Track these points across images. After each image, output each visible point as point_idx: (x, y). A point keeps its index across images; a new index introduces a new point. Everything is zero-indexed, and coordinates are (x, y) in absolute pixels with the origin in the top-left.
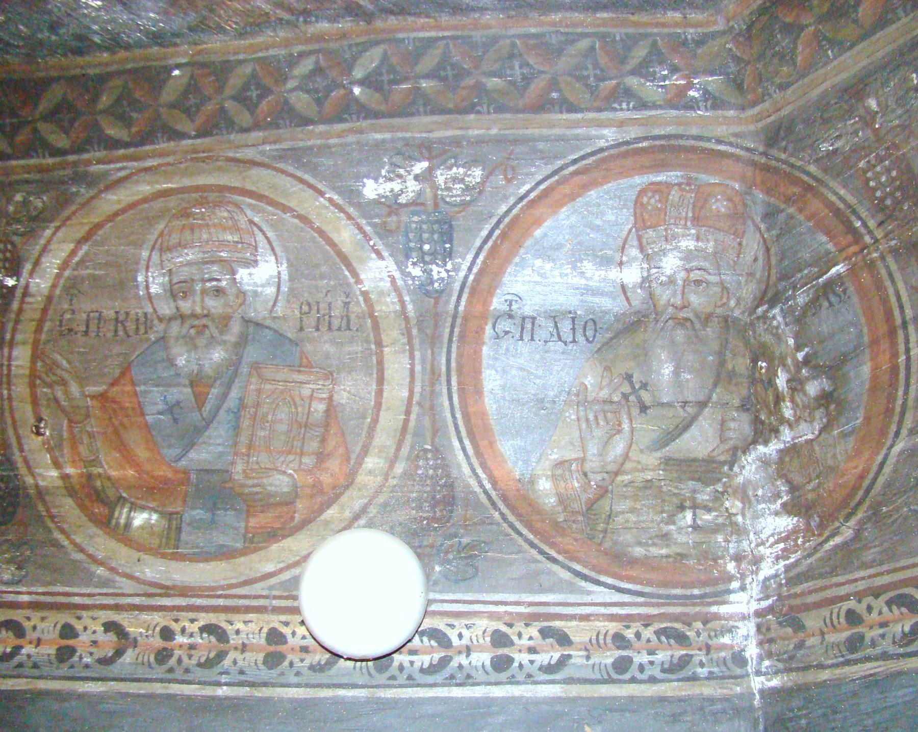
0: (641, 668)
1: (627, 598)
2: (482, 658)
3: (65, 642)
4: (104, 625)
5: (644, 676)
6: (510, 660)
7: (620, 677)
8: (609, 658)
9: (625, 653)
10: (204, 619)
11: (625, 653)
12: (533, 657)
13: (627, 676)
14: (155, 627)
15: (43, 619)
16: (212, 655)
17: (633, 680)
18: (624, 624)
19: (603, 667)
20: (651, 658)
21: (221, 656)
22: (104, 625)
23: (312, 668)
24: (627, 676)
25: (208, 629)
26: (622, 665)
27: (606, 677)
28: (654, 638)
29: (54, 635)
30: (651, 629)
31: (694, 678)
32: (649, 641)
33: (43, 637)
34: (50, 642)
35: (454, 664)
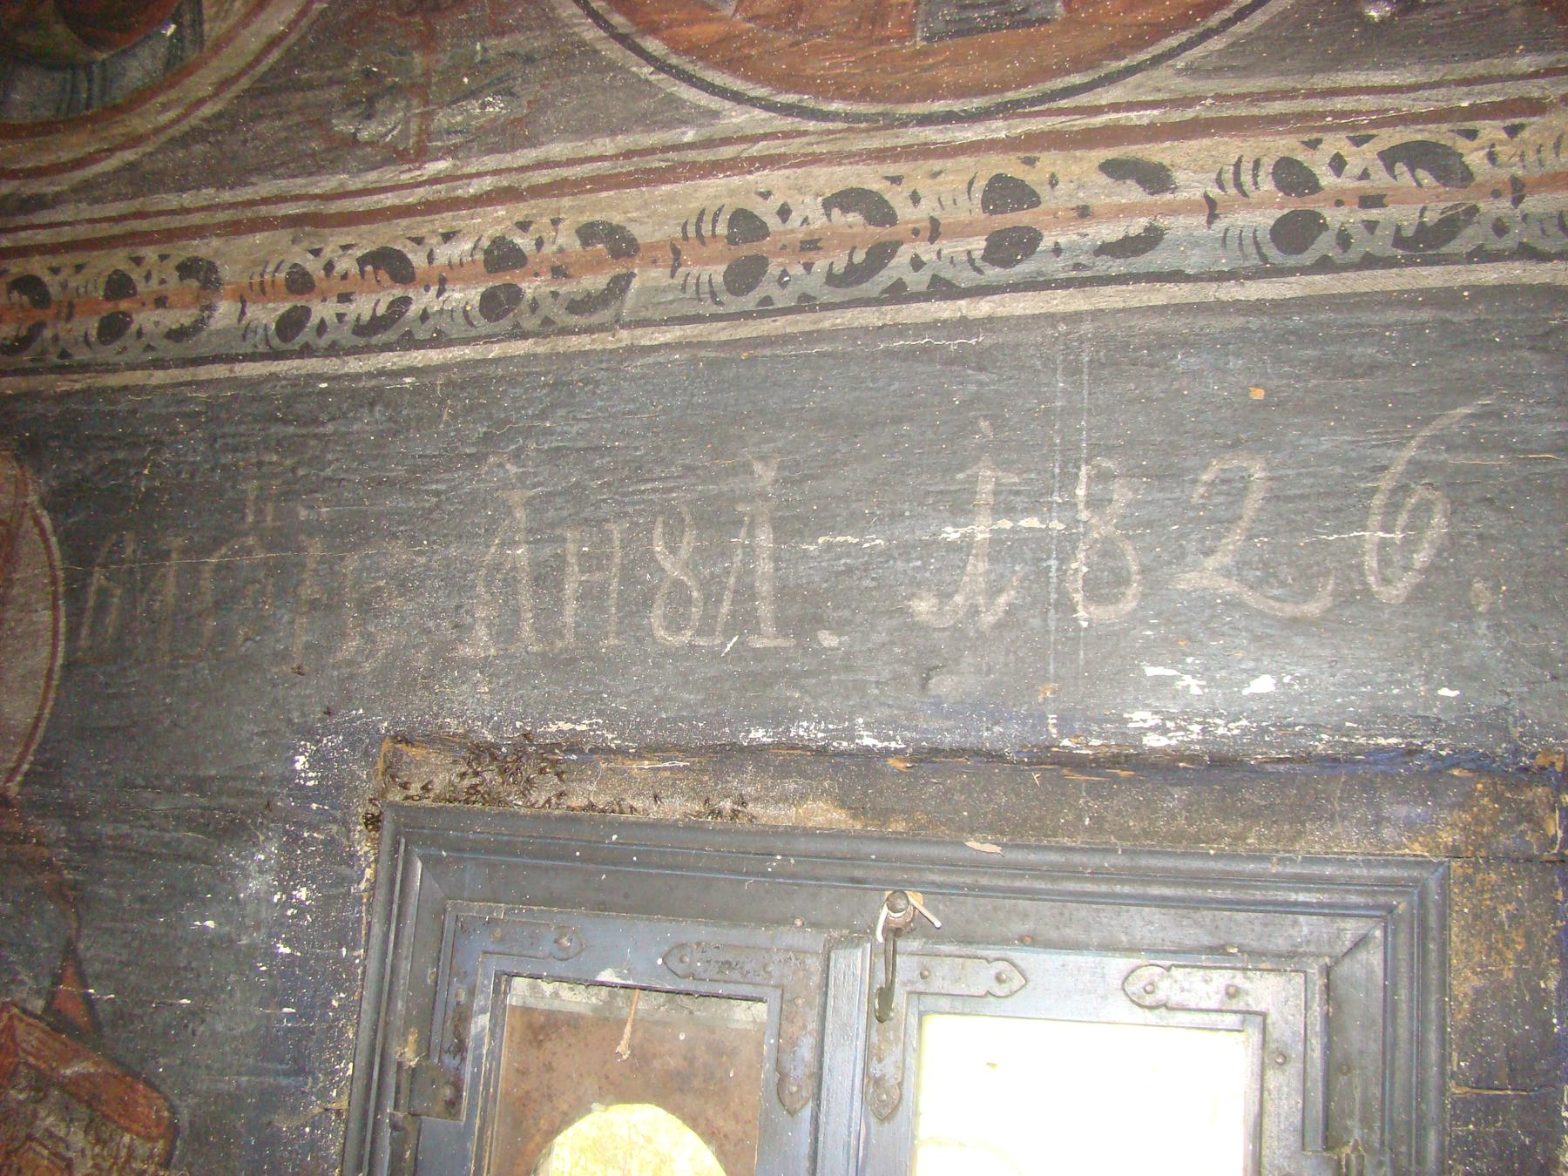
0: (1500, 229)
1: (787, 123)
2: (466, 296)
3: (745, 250)
4: (180, 268)
6: (515, 294)
7: (1292, 261)
8: (266, 314)
9: (300, 302)
10: (368, 239)
11: (300, 302)
12: (1374, 214)
13: (1308, 258)
14: (1237, 174)
15: (79, 268)
16: (859, 257)
17: (1324, 265)
18: (1508, 122)
19: (1248, 241)
20: (341, 308)
21: (881, 254)
22: (180, 268)
23: (832, 279)
24: (1308, 258)
25: (846, 200)
26: (291, 324)
27: (1255, 261)
28: (354, 269)
29: (969, 209)
30: (1370, 150)
31: (897, 293)
32: (345, 277)
33: (945, 218)
34: (964, 231)
35: (414, 310)
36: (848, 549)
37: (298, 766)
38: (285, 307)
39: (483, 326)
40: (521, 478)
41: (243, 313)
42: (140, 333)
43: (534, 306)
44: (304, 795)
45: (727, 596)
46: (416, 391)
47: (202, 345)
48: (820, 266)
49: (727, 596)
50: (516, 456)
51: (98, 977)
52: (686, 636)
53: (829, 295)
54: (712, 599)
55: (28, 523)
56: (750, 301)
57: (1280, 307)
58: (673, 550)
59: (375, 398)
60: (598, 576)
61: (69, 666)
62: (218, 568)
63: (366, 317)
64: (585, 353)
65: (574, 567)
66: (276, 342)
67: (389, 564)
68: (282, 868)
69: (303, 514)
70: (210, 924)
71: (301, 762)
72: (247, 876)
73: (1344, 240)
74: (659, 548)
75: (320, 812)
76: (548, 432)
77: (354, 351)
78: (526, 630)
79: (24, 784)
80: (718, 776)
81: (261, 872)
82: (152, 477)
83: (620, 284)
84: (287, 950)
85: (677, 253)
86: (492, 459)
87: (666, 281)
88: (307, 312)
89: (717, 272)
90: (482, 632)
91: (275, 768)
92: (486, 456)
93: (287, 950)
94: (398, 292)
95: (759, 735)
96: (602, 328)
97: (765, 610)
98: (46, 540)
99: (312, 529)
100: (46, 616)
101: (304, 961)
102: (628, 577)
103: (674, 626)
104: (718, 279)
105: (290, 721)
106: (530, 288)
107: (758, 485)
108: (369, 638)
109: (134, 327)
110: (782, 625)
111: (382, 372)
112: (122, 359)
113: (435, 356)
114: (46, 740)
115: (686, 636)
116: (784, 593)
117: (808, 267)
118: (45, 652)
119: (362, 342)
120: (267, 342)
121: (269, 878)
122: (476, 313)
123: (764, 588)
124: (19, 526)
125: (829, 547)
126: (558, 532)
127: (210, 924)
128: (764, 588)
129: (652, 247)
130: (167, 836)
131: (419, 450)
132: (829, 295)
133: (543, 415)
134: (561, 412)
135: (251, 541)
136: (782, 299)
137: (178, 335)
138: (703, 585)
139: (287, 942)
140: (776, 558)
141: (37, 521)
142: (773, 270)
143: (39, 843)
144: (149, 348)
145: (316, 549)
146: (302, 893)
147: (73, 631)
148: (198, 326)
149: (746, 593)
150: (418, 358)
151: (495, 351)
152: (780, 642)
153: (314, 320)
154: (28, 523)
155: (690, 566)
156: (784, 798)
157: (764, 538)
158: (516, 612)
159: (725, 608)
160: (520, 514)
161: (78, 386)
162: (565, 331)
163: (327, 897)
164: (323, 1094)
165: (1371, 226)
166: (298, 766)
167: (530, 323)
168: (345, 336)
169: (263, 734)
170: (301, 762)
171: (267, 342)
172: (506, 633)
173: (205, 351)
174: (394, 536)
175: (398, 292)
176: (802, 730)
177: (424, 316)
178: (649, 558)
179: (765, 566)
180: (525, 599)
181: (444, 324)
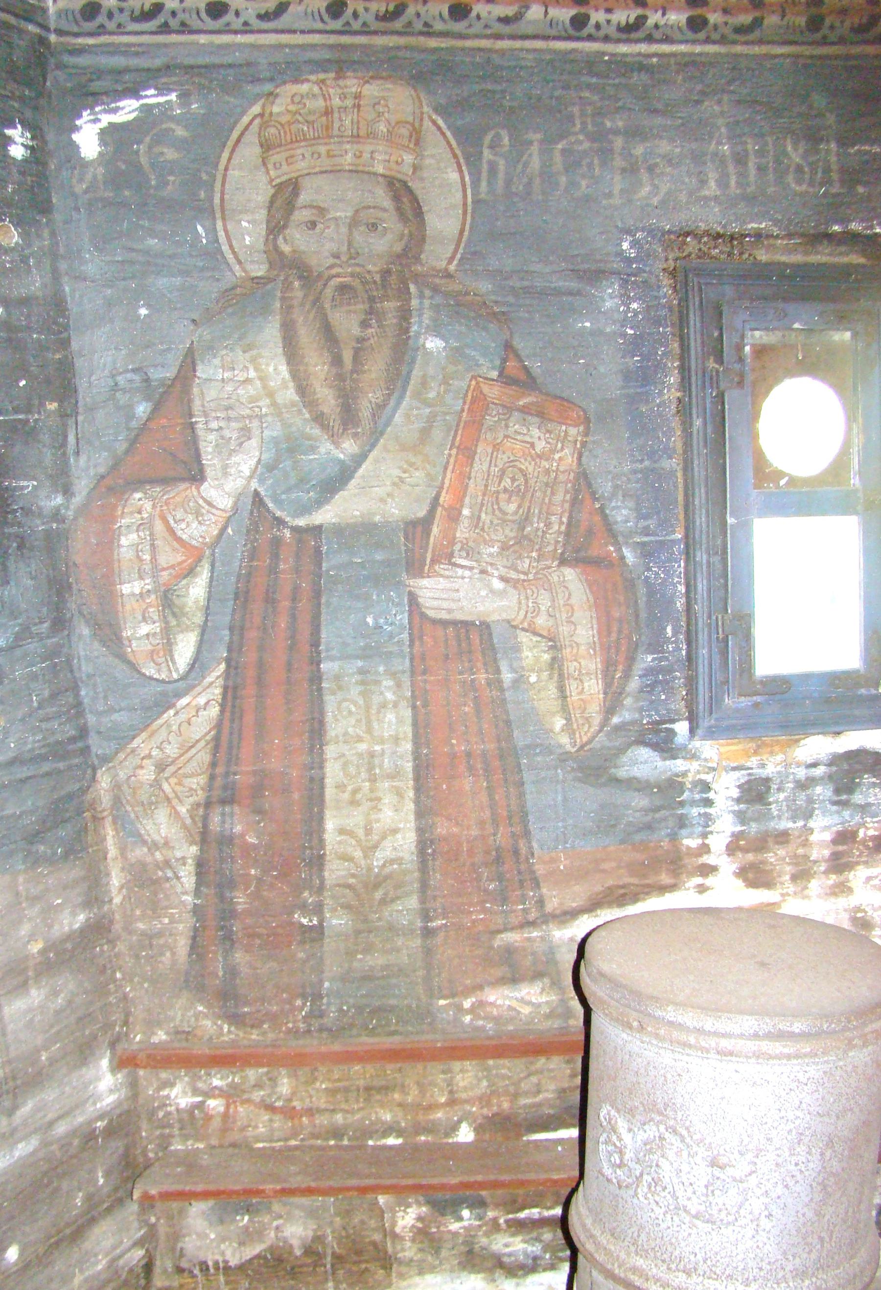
5: (602, 33)
6: (705, 22)
9: (583, 10)
11: (583, 10)
26: (579, 22)
35: (650, 22)
36: (866, 153)
37: (624, 248)
38: (573, 12)
39: (690, 35)
40: (722, 113)
41: (546, 12)
42: (478, 17)
43: (716, 27)
44: (629, 261)
45: (820, 170)
46: (660, 66)
47: (522, 27)
48: (848, 24)
49: (820, 170)
50: (719, 102)
51: (528, 357)
52: (804, 187)
53: (256, 24)
54: (813, 171)
55: (427, 123)
56: (818, 36)
57: (828, 57)
58: (796, 150)
59: (642, 68)
60: (764, 160)
61: (477, 202)
62: (563, 151)
63: (623, 23)
64: (747, 55)
65: (752, 157)
66: (571, 32)
67: (661, 151)
68: (622, 295)
69: (609, 124)
70: (588, 324)
71: (625, 246)
72: (604, 301)
73: (598, 26)
74: (789, 148)
75: (638, 268)
76: (733, 92)
77: (618, 41)
78: (733, 183)
79: (458, 265)
80: (813, 246)
81: (611, 298)
82: (511, 100)
83: (757, 23)
84: (632, 332)
85: (784, 11)
86: (706, 103)
87: (779, 22)
88: (587, 17)
89: (801, 21)
90: (712, 184)
91: (611, 249)
92: (703, 101)
93: (632, 332)
94: (639, 11)
95: (836, 228)
96: (752, 43)
97: (835, 176)
98: (443, 134)
99: (616, 132)
100: (454, 176)
101: (641, 337)
102: (778, 162)
103: (799, 182)
104: (803, 24)
105: (617, 227)
106: (714, 18)
107: (828, 123)
108: (656, 187)
109: (474, 14)
110: (842, 181)
111: (639, 54)
112: (471, 31)
113: (666, 48)
114: (469, 241)
115: (804, 187)
116: (842, 170)
117: (842, 22)
118: (459, 195)
119: (624, 36)
120: (566, 31)
121: (616, 300)
122: (685, 28)
123: (834, 167)
124: (421, 125)
125: (859, 151)
126: (744, 139)
127: (588, 324)
128: (834, 167)
129: (771, 5)
130: (553, 285)
131: (667, 96)
132: (375, 25)
133: (729, 83)
134: (737, 83)
135: (581, 137)
136: (833, 37)
137: (505, 20)
138: (810, 164)
139: (631, 328)
140: (838, 155)
141: (434, 123)
142: (828, 22)
143: (475, 294)
144: (486, 26)
145: (619, 142)
146: (634, 306)
147: (476, 183)
148: (518, 17)
149: (827, 170)
150: (655, 48)
151: (698, 49)
152: (842, 191)
153: (592, 21)
154: (427, 123)
155: (805, 156)
156: (841, 254)
157: (833, 145)
158: (728, 175)
159: (819, 175)
160: (723, 130)
161: (443, 45)
162: (734, 42)
163: (648, 306)
164: (661, 393)
165: (608, 22)
166: (624, 248)
167: (715, 36)
168: (612, 31)
169: (602, 233)
170: (625, 246)
171: (566, 31)
172: (723, 183)
173: (530, 31)
174: (661, 138)
175: (757, 14)
176: (854, 226)
177: (656, 26)
178: (785, 153)
179: (833, 159)
180: (731, 168)
181: (669, 32)
